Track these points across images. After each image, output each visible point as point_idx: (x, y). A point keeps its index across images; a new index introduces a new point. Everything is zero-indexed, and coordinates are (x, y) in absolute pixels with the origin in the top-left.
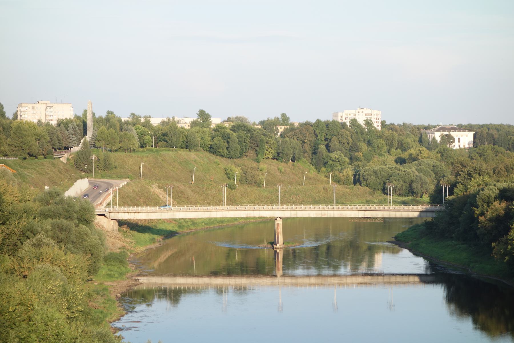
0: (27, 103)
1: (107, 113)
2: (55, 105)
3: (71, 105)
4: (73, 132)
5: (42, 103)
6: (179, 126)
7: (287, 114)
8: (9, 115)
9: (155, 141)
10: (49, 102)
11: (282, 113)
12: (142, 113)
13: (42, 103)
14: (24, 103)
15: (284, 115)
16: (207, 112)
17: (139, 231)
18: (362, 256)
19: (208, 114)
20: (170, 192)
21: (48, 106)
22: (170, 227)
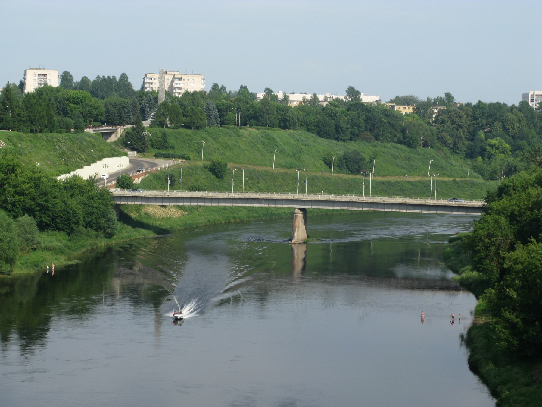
0: (154, 74)
1: (240, 87)
2: (184, 77)
3: (202, 77)
4: (147, 105)
5: (170, 74)
6: (5, 87)
7: (67, 71)
8: (137, 87)
9: (238, 121)
10: (178, 73)
11: (446, 92)
12: (469, 101)
13: (170, 74)
14: (149, 73)
15: (448, 95)
16: (357, 89)
17: (134, 227)
18: (6, 267)
19: (358, 91)
20: (366, 186)
21: (176, 77)
22: (166, 225)
